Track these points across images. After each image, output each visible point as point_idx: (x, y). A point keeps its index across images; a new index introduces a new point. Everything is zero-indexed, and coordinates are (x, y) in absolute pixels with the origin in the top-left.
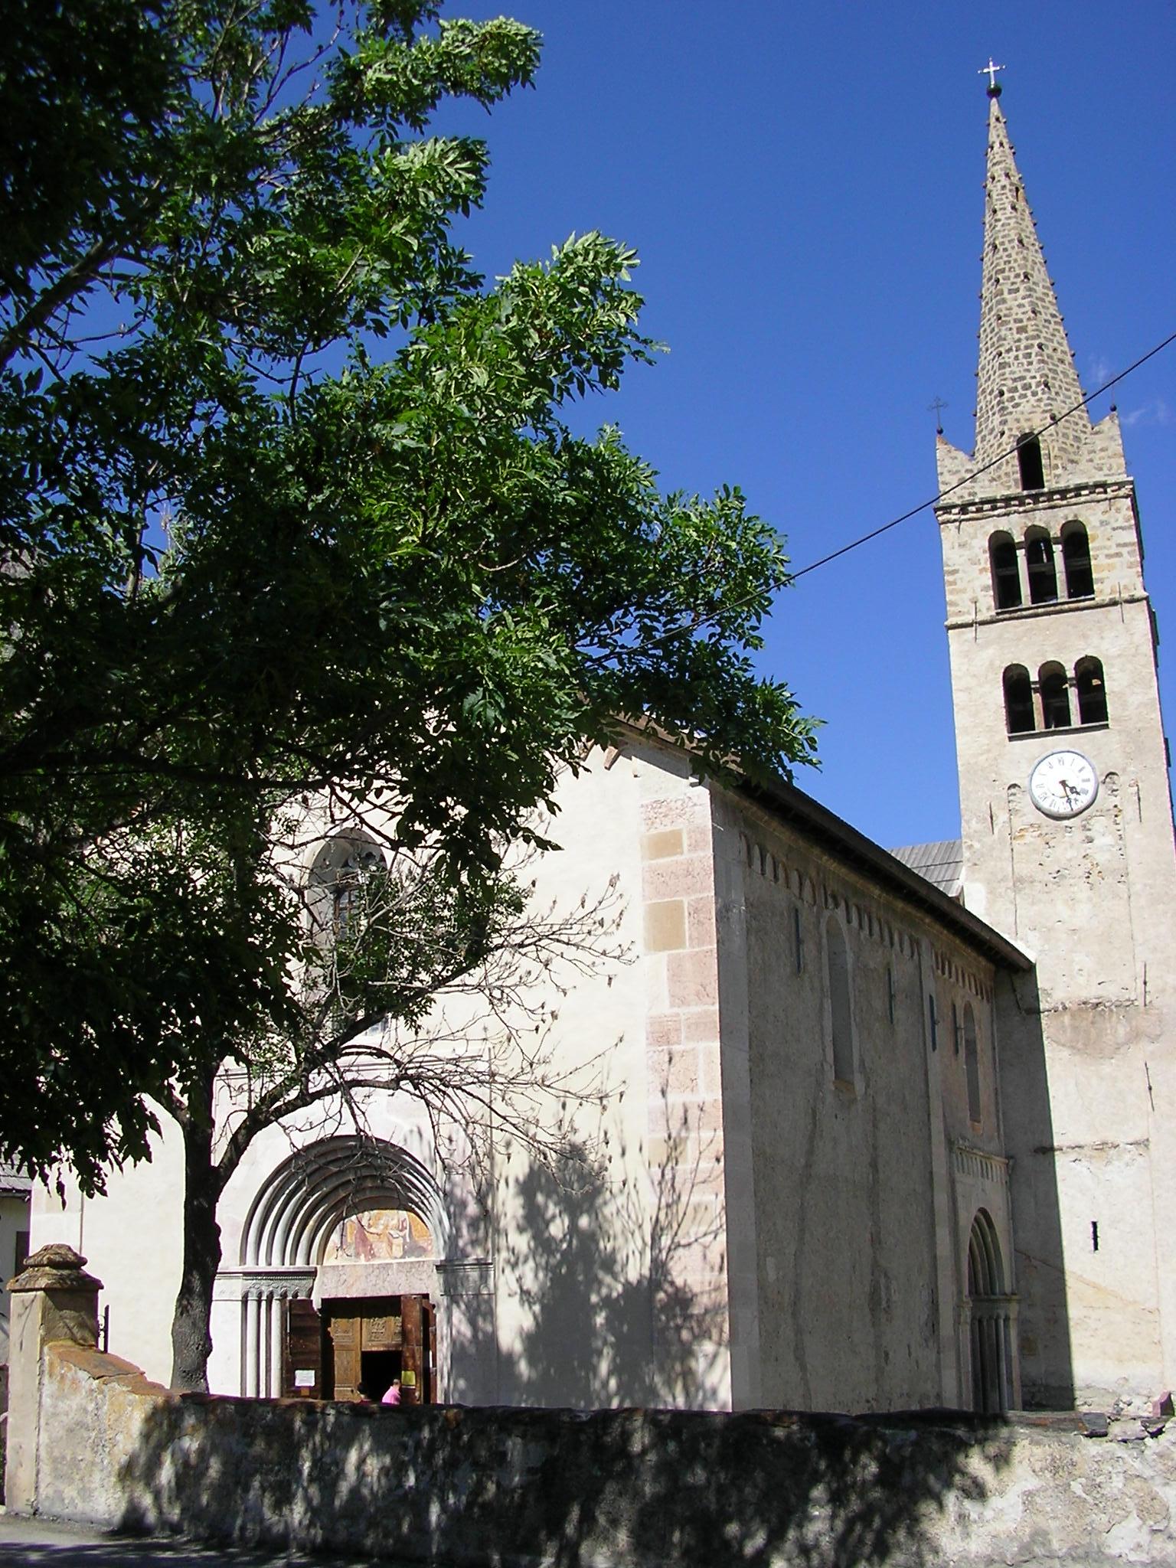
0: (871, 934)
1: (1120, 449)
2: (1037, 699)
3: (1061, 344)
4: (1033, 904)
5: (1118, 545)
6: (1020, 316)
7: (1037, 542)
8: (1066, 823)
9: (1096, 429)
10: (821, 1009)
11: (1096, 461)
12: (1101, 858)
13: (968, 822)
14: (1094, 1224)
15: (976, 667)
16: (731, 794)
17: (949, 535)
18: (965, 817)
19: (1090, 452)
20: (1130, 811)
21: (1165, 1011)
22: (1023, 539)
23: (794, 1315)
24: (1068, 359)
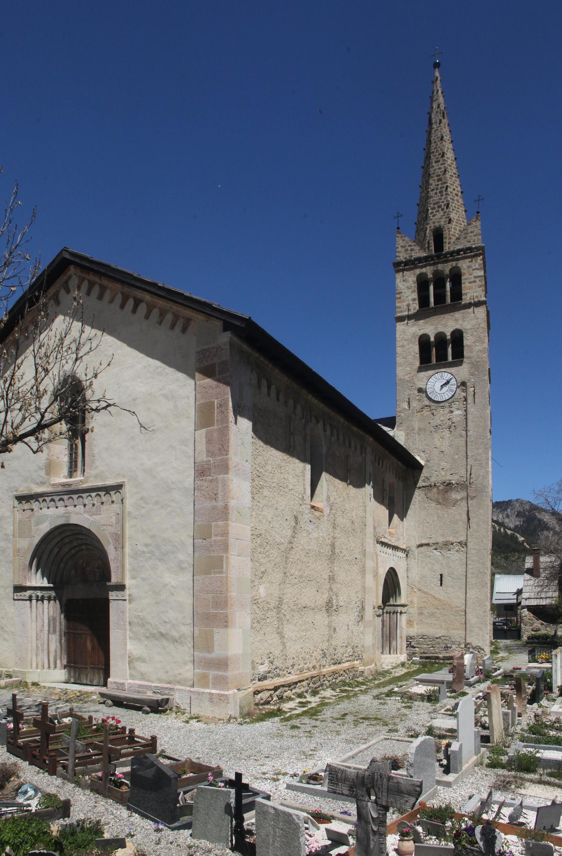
0: (338, 440)
1: (480, 232)
5: (475, 277)
6: (439, 173)
8: (442, 404)
11: (468, 238)
14: (441, 575)
15: (407, 336)
20: (470, 399)
22: (432, 276)
24: (460, 194)
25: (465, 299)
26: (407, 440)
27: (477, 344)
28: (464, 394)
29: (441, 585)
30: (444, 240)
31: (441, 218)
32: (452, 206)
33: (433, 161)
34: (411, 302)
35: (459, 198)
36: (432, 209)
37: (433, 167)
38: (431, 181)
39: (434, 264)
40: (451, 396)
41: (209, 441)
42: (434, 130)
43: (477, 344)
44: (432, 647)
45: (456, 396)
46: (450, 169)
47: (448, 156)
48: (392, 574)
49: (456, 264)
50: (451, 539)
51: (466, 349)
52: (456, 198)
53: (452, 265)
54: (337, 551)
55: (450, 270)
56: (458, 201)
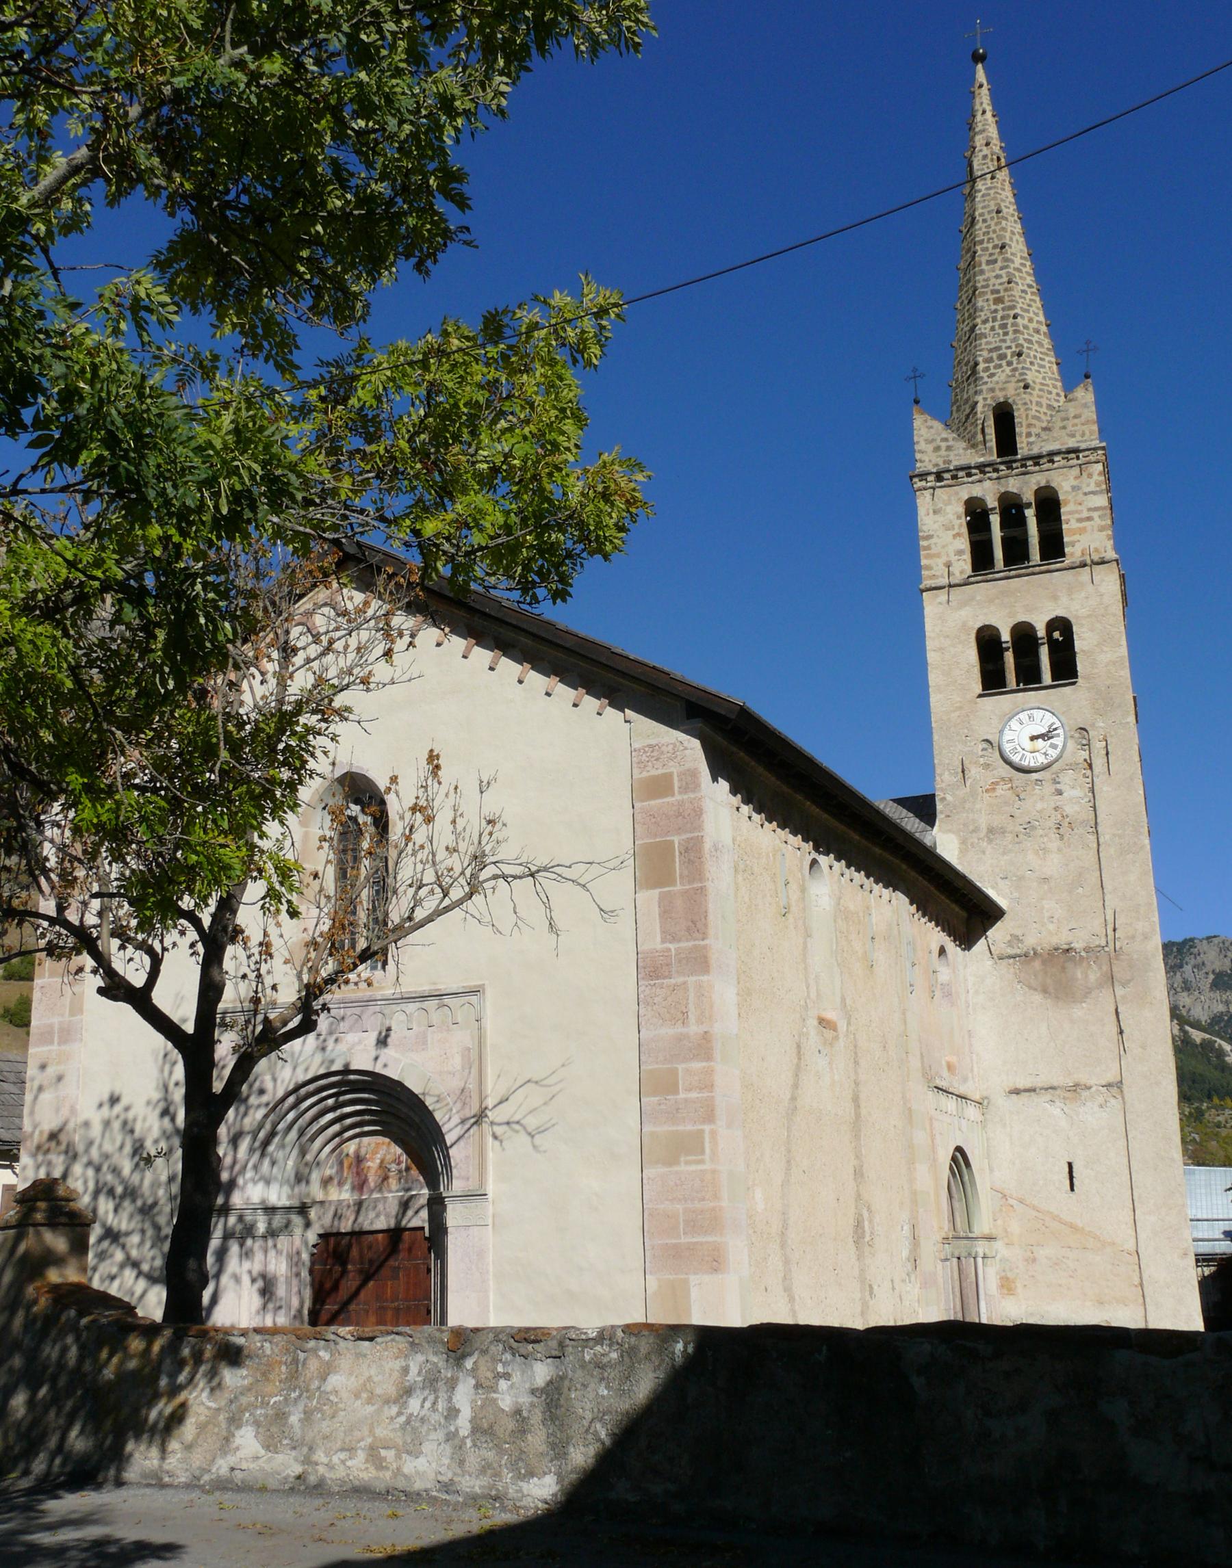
2: (1009, 657)
3: (1037, 314)
4: (1004, 853)
5: (1089, 510)
6: (997, 287)
7: (1011, 509)
8: (1035, 776)
9: (1070, 396)
11: (1070, 428)
12: (1069, 810)
13: (941, 775)
16: (720, 739)
17: (924, 502)
18: (938, 771)
19: (1064, 419)
20: (1099, 763)
21: (1135, 956)
22: (996, 504)
23: (783, 1245)
24: (1044, 329)
25: (1072, 554)
26: (963, 852)
28: (1085, 755)
31: (1006, 382)
32: (1028, 356)
34: (954, 558)
36: (990, 360)
37: (982, 272)
41: (666, 912)
42: (979, 195)
46: (1021, 278)
47: (1013, 250)
52: (1036, 338)
55: (1038, 492)
56: (1040, 344)
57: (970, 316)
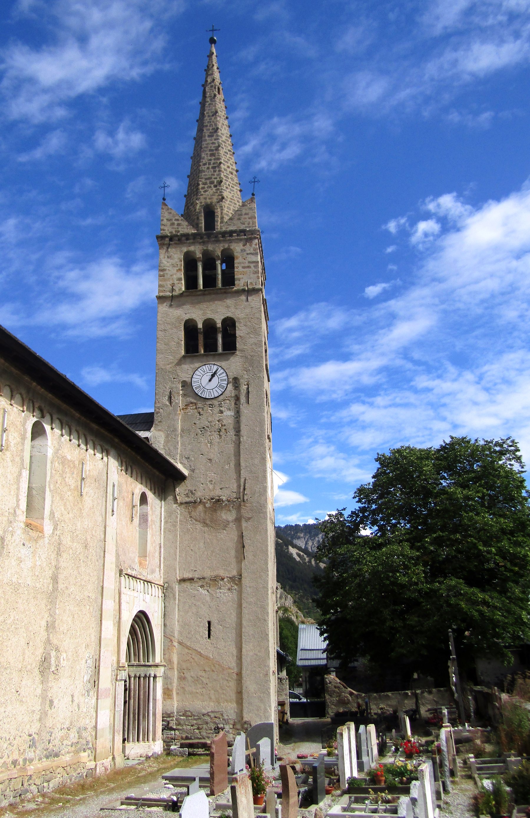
5: (249, 262)
6: (212, 148)
8: (210, 402)
10: (20, 474)
20: (243, 399)
22: (201, 256)
26: (167, 442)
27: (252, 336)
29: (209, 637)
30: (216, 219)
32: (225, 184)
33: (207, 135)
35: (234, 176)
36: (205, 184)
37: (206, 140)
38: (203, 155)
39: (204, 243)
40: (220, 393)
42: (208, 104)
43: (252, 336)
44: (198, 729)
45: (227, 393)
46: (225, 146)
47: (223, 132)
48: (142, 619)
49: (229, 246)
50: (222, 573)
51: (238, 340)
53: (224, 246)
54: (61, 586)
55: (223, 252)
57: (197, 162)
